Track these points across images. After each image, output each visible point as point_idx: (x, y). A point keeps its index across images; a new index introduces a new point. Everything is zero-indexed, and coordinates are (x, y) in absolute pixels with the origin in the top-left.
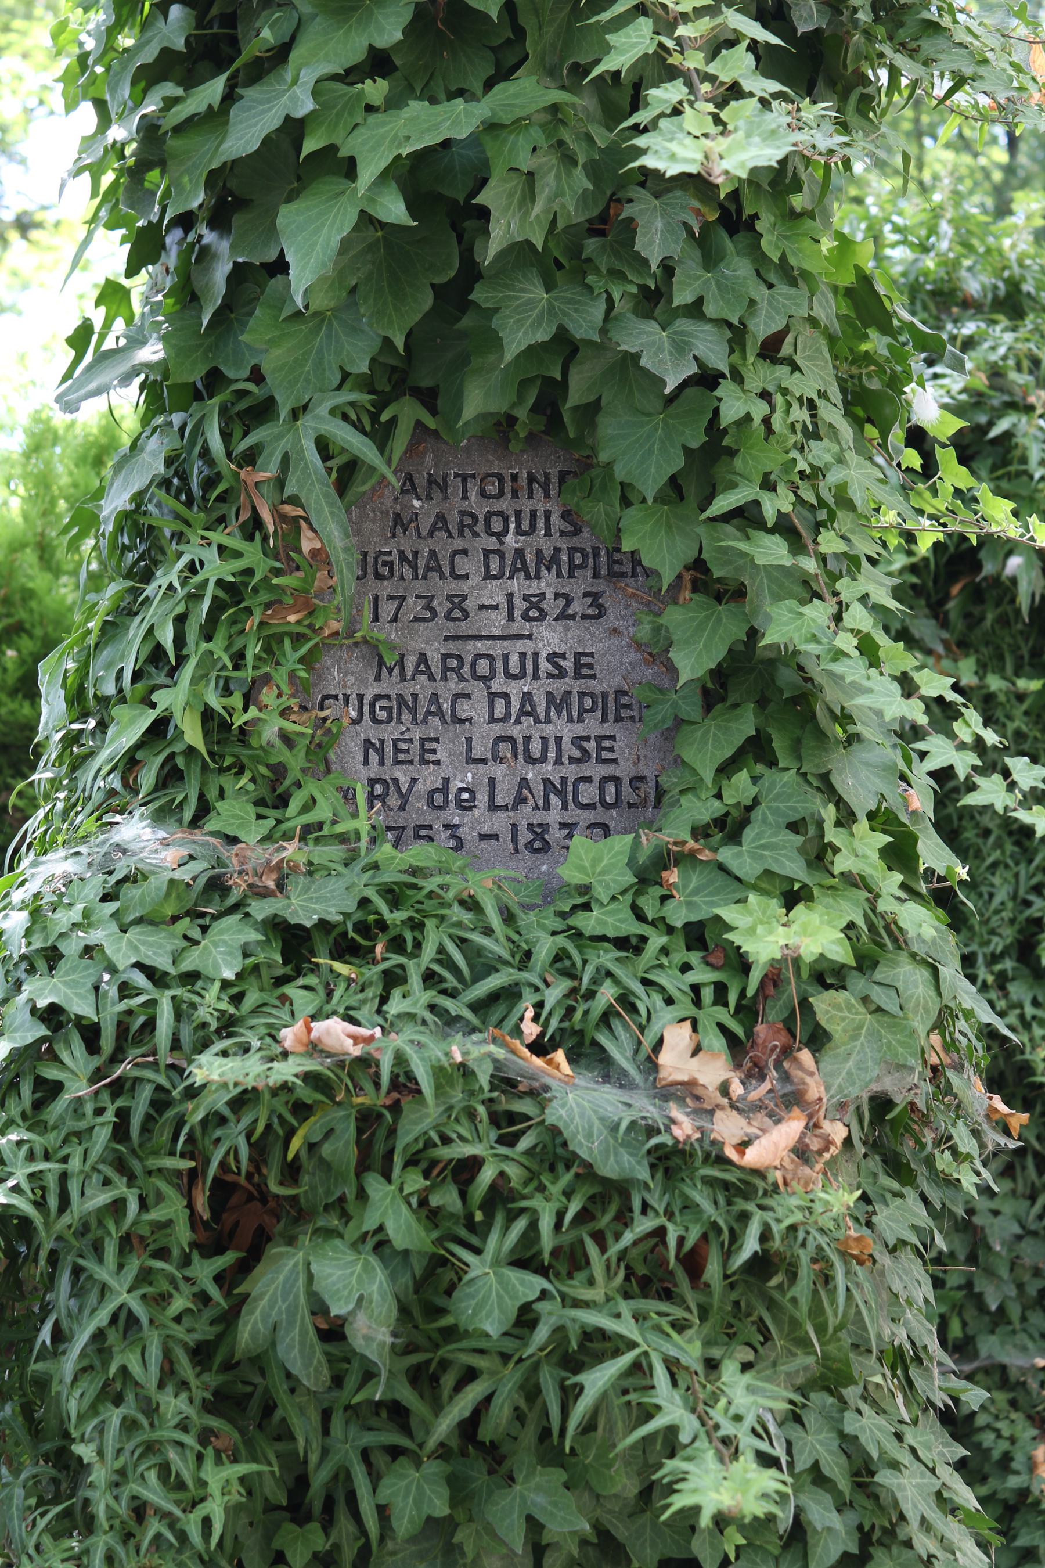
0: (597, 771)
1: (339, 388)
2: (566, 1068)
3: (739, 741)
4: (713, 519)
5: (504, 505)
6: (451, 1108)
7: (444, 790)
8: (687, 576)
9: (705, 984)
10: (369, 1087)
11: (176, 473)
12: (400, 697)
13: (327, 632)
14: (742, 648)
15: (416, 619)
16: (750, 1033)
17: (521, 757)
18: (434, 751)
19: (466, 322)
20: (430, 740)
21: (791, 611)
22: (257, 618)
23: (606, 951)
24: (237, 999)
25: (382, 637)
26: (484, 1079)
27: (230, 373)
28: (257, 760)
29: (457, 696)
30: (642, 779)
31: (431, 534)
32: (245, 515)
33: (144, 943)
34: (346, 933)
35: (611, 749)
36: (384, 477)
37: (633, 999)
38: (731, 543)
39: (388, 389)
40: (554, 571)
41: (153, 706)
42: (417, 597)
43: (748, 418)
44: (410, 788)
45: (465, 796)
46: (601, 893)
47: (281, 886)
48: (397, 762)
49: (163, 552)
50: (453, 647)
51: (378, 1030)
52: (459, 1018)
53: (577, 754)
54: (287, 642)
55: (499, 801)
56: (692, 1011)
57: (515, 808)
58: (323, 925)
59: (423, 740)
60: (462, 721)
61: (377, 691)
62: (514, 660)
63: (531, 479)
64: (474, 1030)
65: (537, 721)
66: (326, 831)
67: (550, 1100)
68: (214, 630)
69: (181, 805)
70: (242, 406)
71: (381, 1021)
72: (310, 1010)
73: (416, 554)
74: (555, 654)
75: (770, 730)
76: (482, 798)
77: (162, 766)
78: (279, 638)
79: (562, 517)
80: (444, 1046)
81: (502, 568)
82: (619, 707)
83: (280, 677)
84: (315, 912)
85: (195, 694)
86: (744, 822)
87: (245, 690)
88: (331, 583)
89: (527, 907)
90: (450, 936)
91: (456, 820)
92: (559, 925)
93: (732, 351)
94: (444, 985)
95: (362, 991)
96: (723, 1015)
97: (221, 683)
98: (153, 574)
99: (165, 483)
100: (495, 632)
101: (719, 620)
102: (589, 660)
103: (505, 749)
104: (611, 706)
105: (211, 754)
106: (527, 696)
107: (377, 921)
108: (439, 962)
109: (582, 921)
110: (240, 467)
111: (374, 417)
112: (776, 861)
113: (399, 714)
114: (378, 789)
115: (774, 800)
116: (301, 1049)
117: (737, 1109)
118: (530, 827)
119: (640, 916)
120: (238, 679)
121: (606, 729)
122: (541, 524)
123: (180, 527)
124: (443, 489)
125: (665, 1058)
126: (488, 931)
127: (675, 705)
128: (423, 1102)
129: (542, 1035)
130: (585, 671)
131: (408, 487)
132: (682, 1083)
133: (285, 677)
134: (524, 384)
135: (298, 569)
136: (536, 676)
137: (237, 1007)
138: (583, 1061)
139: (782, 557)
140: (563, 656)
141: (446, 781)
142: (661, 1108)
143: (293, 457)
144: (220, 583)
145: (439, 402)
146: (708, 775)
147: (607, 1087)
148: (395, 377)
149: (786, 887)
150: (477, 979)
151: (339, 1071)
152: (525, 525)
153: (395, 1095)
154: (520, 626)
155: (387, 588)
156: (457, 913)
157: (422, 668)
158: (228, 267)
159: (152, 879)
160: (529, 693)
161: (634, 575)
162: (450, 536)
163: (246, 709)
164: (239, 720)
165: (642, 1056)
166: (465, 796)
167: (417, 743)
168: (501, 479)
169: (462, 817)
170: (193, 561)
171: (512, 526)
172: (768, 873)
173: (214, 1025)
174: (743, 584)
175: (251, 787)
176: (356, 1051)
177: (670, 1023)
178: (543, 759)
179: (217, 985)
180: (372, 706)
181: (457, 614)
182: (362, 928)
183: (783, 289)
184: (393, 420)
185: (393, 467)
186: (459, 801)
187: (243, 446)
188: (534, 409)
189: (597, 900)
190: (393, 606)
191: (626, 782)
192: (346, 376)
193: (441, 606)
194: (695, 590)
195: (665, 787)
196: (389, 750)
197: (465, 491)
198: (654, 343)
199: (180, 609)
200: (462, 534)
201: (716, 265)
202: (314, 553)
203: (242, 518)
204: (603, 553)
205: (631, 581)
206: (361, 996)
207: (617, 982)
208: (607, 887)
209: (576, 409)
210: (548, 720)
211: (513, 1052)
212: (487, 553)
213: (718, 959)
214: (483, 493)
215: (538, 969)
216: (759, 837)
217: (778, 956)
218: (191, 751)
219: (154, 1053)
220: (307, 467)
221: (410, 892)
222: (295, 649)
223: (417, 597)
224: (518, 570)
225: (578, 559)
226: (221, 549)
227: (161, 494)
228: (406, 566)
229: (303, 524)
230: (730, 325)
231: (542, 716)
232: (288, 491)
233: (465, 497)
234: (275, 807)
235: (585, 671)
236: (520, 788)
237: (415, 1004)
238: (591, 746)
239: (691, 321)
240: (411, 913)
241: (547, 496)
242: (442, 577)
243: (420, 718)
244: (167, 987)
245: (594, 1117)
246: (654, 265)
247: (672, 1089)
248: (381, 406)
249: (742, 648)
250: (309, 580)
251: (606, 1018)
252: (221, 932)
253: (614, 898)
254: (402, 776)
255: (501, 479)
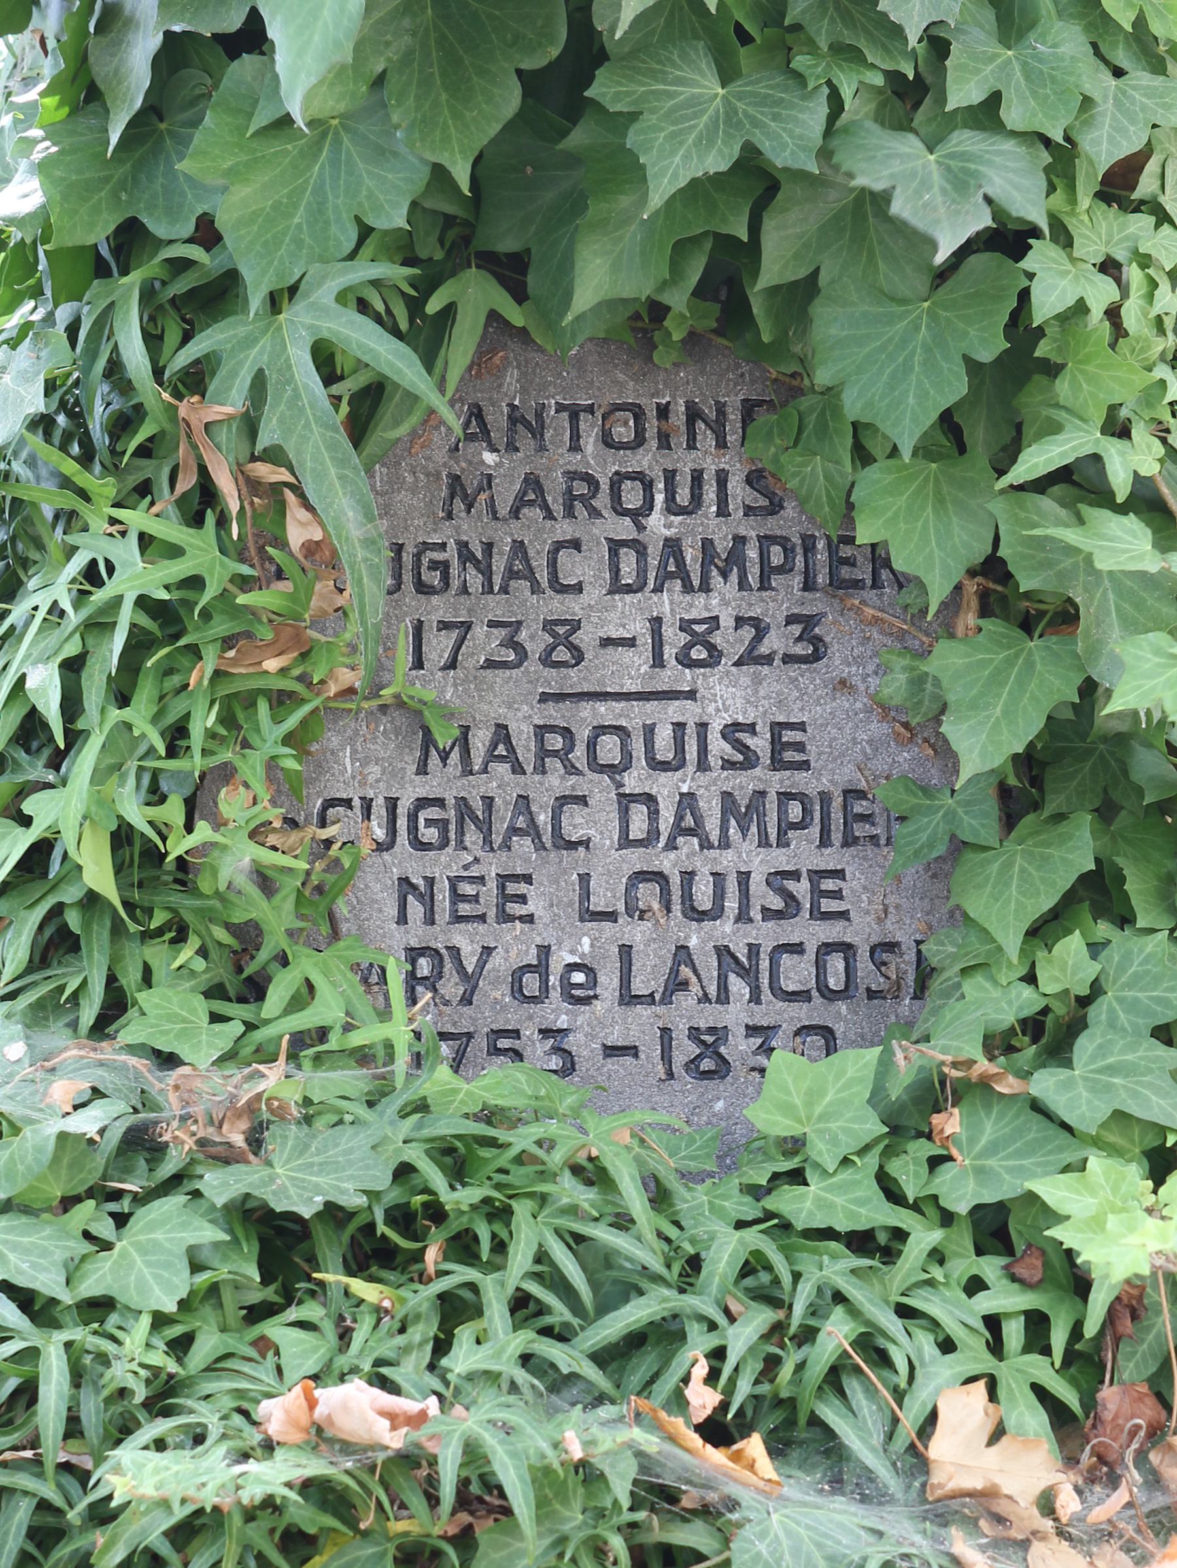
0: (812, 934)
1: (352, 256)
2: (766, 1466)
3: (1065, 881)
4: (1021, 488)
5: (645, 460)
6: (563, 1540)
7: (541, 967)
8: (971, 587)
9: (1008, 1315)
10: (417, 1503)
11: (62, 405)
12: (462, 802)
13: (333, 689)
14: (1069, 714)
15: (490, 664)
16: (1090, 1403)
17: (677, 908)
18: (522, 899)
19: (578, 137)
20: (515, 878)
21: (1158, 652)
22: (209, 664)
23: (834, 1257)
24: (181, 1346)
25: (429, 695)
26: (621, 1489)
27: (158, 227)
28: (209, 916)
29: (563, 800)
30: (891, 947)
31: (515, 513)
32: (187, 481)
33: (15, 1247)
34: (371, 1227)
35: (837, 895)
36: (432, 412)
37: (881, 1342)
38: (1052, 531)
39: (439, 255)
40: (734, 577)
41: (26, 821)
42: (492, 624)
43: (1081, 308)
44: (481, 964)
45: (578, 977)
46: (823, 1152)
47: (255, 1142)
48: (459, 919)
49: (40, 546)
50: (555, 714)
51: (433, 1401)
52: (573, 1377)
53: (777, 903)
54: (263, 707)
55: (639, 986)
56: (986, 1362)
57: (666, 1000)
58: (333, 1213)
59: (503, 879)
60: (572, 845)
61: (422, 792)
62: (664, 736)
63: (693, 414)
64: (600, 1399)
65: (706, 844)
66: (333, 1043)
67: (739, 1525)
68: (134, 685)
69: (75, 996)
70: (180, 287)
71: (438, 1386)
72: (312, 1365)
73: (489, 547)
74: (736, 726)
75: (1120, 861)
76: (609, 981)
77: (41, 927)
78: (249, 701)
79: (749, 481)
80: (549, 1428)
81: (642, 573)
82: (851, 818)
83: (251, 767)
84: (317, 1189)
85: (105, 802)
86: (1075, 1026)
87: (188, 792)
88: (340, 601)
89: (689, 1177)
90: (558, 1232)
91: (563, 1022)
92: (750, 1210)
93: (1051, 189)
94: (548, 1320)
95: (402, 1330)
96: (1043, 1370)
97: (146, 780)
98: (20, 583)
99: (42, 424)
100: (631, 686)
101: (1030, 665)
102: (796, 736)
103: (648, 894)
104: (837, 816)
105: (127, 905)
106: (688, 801)
107: (425, 1205)
108: (538, 1277)
109: (786, 1201)
110: (179, 396)
111: (415, 306)
112: (1135, 1095)
113: (461, 832)
114: (424, 967)
115: (1129, 986)
116: (297, 1437)
117: (1069, 1538)
118: (694, 1033)
119: (893, 1194)
120: (175, 774)
121: (829, 859)
122: (710, 493)
123: (69, 501)
124: (538, 432)
125: (939, 1448)
126: (623, 1222)
127: (950, 816)
128: (515, 1530)
129: (724, 1406)
130: (789, 755)
131: (474, 428)
132: (971, 1494)
133: (260, 770)
134: (682, 249)
135: (280, 575)
136: (703, 765)
137: (179, 1361)
138: (795, 1454)
139: (1141, 557)
140: (751, 728)
141: (545, 951)
142: (936, 1539)
143: (272, 377)
144: (142, 602)
145: (530, 279)
146: (1011, 941)
147: (839, 1502)
148: (451, 235)
149: (1152, 1142)
150: (604, 1307)
151: (365, 1477)
152: (683, 496)
153: (464, 1518)
154: (674, 676)
155: (438, 608)
156: (569, 1190)
157: (501, 750)
158: (154, 42)
159: (27, 1131)
160: (691, 795)
161: (876, 584)
162: (550, 515)
163: (189, 828)
164: (177, 847)
165: (900, 1443)
166: (578, 977)
167: (492, 884)
168: (638, 413)
169: (573, 1015)
170: (93, 563)
171: (659, 498)
172: (1120, 1117)
173: (141, 1393)
174: (1070, 600)
175: (200, 964)
176: (396, 1441)
177: (949, 1385)
178: (716, 912)
179: (145, 1321)
180: (413, 818)
181: (562, 654)
182: (402, 1218)
183: (1140, 77)
184: (449, 312)
185: (449, 394)
186: (567, 986)
187: (184, 358)
188: (699, 292)
189: (817, 1165)
190: (447, 641)
191: (863, 953)
192: (365, 232)
193: (534, 640)
194: (985, 612)
195: (934, 962)
196: (443, 896)
197: (575, 436)
198: (913, 174)
199: (72, 649)
200: (570, 513)
201: (1022, 34)
202: (311, 548)
203: (183, 485)
204: (820, 545)
205: (870, 595)
206: (400, 1340)
207: (854, 1312)
208: (834, 1141)
209: (773, 291)
210: (725, 843)
211: (672, 1439)
212: (615, 546)
213: (1031, 1269)
214: (607, 441)
215: (714, 1289)
216: (1103, 1050)
217: (1146, 1271)
218: (92, 900)
219: (34, 1443)
220: (297, 396)
221: (485, 1153)
222: (277, 720)
223: (492, 624)
224: (671, 576)
225: (777, 556)
226: (145, 540)
227: (36, 441)
228: (471, 570)
229: (290, 496)
230: (1047, 142)
231: (714, 837)
232: (265, 440)
233: (575, 447)
234: (242, 1000)
235: (789, 755)
236: (676, 964)
237: (498, 1355)
238: (801, 889)
239: (978, 135)
240: (489, 1192)
241: (722, 444)
242: (536, 588)
243: (497, 840)
244: (56, 1325)
245: (817, 1555)
246: (913, 37)
247: (954, 1504)
248: (427, 286)
249: (1069, 714)
250: (300, 598)
251: (835, 1378)
252: (151, 1227)
253: (846, 1161)
254: (467, 941)
255: (638, 413)
